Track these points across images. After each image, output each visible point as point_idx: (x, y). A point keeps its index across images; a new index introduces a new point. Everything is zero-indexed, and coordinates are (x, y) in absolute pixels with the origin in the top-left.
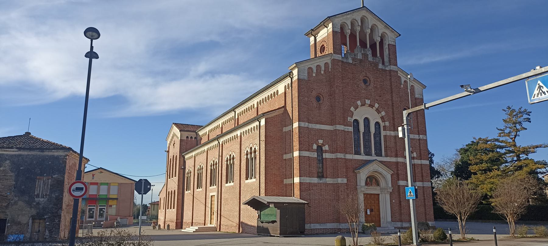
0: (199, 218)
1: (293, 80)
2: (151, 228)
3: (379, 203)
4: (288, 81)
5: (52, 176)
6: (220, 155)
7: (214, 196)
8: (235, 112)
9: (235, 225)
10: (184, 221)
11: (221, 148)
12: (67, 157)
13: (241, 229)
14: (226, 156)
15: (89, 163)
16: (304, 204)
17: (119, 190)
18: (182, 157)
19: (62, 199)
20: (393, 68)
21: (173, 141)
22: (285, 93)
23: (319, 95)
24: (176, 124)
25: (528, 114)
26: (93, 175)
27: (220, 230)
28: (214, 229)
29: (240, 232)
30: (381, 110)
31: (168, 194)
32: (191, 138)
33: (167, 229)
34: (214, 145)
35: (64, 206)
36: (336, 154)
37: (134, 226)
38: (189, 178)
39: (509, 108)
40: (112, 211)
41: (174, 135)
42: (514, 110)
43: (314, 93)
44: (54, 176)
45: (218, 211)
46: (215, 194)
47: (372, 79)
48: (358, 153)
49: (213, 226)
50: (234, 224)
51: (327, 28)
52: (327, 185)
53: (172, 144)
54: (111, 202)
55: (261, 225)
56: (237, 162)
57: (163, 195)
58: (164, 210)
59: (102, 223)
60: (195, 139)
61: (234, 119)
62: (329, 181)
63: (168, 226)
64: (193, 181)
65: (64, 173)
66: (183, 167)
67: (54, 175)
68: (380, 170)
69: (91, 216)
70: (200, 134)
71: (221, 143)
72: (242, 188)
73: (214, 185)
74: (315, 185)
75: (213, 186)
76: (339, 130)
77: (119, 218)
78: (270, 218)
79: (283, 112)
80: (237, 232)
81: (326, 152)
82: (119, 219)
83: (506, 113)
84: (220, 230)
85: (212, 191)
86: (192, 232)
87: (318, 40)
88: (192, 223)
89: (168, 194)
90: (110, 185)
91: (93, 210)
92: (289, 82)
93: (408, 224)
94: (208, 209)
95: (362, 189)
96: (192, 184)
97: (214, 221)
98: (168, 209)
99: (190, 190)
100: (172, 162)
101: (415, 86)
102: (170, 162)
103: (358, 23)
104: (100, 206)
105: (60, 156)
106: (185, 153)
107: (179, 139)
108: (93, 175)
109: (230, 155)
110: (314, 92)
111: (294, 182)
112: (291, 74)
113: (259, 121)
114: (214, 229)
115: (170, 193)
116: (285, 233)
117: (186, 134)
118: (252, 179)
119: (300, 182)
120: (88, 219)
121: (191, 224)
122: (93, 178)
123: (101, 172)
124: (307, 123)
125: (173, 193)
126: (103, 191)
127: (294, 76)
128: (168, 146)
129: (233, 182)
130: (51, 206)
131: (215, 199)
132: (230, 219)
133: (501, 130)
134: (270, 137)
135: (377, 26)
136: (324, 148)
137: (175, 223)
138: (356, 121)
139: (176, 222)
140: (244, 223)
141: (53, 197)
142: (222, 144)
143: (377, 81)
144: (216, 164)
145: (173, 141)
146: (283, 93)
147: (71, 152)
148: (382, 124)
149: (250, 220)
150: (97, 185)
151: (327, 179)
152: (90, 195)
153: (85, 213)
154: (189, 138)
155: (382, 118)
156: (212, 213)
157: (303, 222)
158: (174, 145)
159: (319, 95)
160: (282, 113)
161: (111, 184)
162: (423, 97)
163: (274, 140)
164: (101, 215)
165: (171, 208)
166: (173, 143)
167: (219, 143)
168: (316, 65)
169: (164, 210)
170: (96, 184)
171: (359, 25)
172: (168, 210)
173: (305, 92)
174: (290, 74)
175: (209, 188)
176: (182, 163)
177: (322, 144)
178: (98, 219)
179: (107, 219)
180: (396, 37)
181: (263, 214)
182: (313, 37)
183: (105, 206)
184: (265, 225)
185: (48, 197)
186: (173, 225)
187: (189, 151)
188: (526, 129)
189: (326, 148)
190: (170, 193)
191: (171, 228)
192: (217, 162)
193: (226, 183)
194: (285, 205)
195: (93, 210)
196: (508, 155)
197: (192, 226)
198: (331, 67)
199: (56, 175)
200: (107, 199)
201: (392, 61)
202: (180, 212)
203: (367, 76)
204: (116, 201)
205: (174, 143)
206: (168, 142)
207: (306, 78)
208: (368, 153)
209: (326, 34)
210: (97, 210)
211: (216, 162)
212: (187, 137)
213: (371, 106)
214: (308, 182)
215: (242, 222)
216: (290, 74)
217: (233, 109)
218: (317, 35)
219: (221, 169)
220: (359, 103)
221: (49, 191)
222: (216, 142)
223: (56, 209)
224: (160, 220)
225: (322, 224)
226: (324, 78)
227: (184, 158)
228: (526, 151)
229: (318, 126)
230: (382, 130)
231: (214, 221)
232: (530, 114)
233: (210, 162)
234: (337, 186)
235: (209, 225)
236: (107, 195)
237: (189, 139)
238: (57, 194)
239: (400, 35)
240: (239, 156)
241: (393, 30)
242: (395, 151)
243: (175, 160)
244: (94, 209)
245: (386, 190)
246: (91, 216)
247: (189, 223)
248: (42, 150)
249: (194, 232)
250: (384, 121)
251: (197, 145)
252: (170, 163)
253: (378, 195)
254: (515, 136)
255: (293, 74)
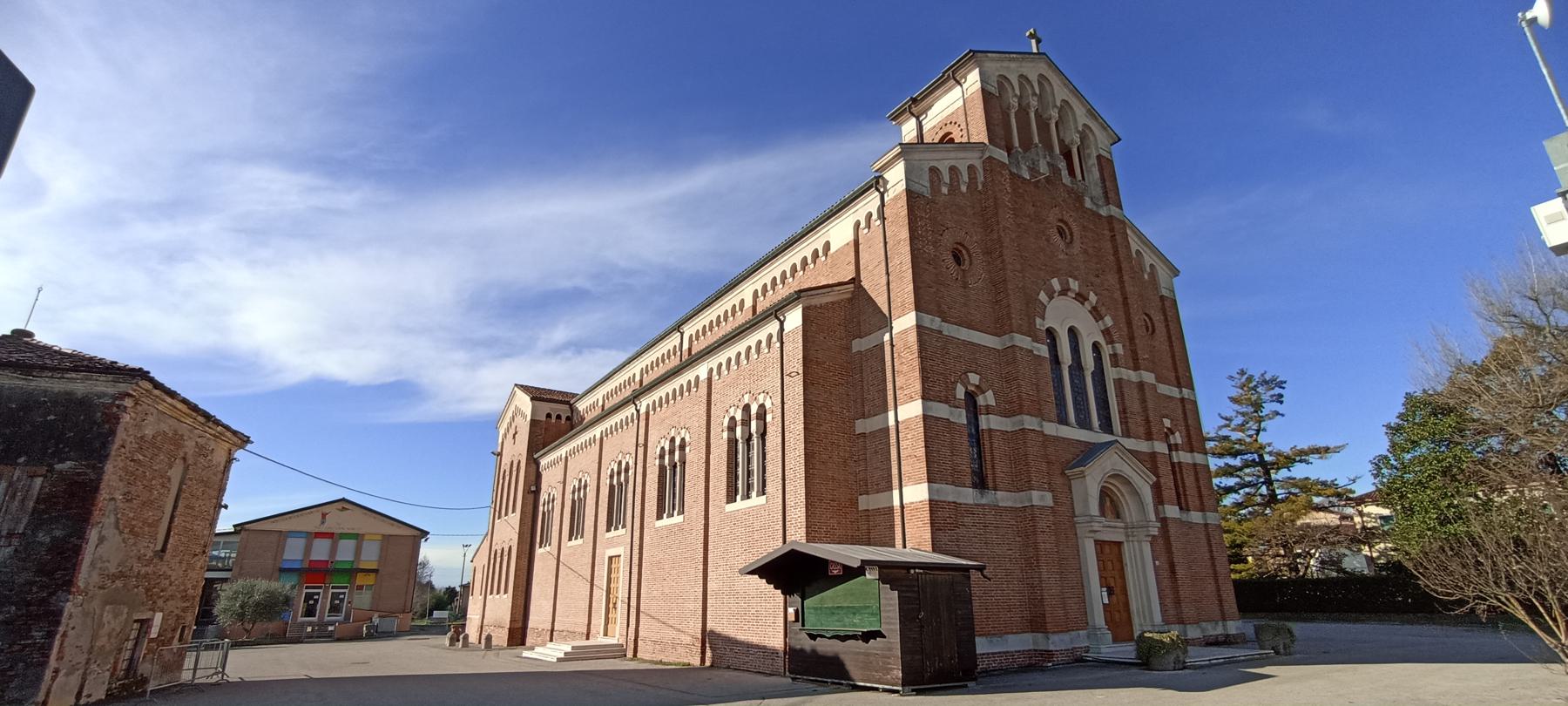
0: (572, 616)
1: (886, 199)
2: (446, 640)
3: (1122, 569)
4: (871, 202)
5: (51, 466)
6: (641, 440)
7: (619, 556)
8: (682, 334)
9: (687, 639)
10: (531, 624)
11: (642, 424)
12: (128, 402)
13: (709, 654)
14: (658, 442)
15: (249, 447)
16: (966, 569)
17: (383, 550)
18: (533, 462)
19: (77, 551)
20: (1114, 210)
21: (513, 427)
22: (856, 243)
23: (960, 248)
24: (522, 386)
25: (1281, 384)
26: (324, 516)
27: (635, 654)
28: (618, 651)
29: (708, 663)
30: (1103, 310)
31: (493, 556)
32: (559, 417)
33: (486, 647)
34: (622, 420)
35: (85, 575)
36: (1019, 417)
37: (412, 635)
38: (549, 514)
39: (1242, 373)
40: (363, 600)
41: (518, 412)
42: (1250, 379)
43: (948, 240)
44: (58, 467)
45: (629, 598)
46: (621, 550)
47: (1075, 229)
48: (1063, 420)
49: (614, 641)
50: (683, 637)
51: (961, 86)
52: (996, 508)
53: (510, 436)
54: (361, 579)
55: (807, 644)
56: (694, 456)
57: (483, 559)
58: (482, 598)
59: (331, 628)
60: (568, 422)
61: (679, 353)
62: (1004, 498)
63: (489, 638)
64: (559, 521)
65: (104, 458)
66: (533, 488)
67: (62, 461)
68: (1128, 471)
69: (310, 612)
70: (580, 409)
71: (643, 410)
72: (711, 530)
73: (620, 527)
74: (969, 510)
75: (616, 528)
76: (1021, 349)
77: (376, 615)
78: (846, 620)
79: (849, 296)
80: (696, 662)
81: (988, 410)
82: (376, 620)
83: (1233, 383)
84: (635, 654)
85: (612, 543)
86: (555, 660)
87: (925, 129)
88: (552, 631)
89: (492, 556)
90: (363, 540)
91: (316, 597)
92: (877, 202)
93: (1199, 631)
94: (600, 595)
95: (1093, 524)
96: (556, 528)
97: (618, 628)
98: (491, 593)
99: (549, 545)
100: (507, 478)
101: (1158, 268)
102: (504, 478)
103: (1032, 87)
104: (333, 588)
105: (96, 395)
106: (542, 452)
107: (529, 418)
108: (324, 516)
109: (673, 440)
110: (947, 235)
111: (904, 502)
112: (881, 181)
113: (779, 320)
114: (618, 652)
115: (499, 555)
116: (918, 679)
117: (547, 407)
118: (735, 501)
119: (930, 500)
120: (300, 619)
121: (549, 632)
122: (323, 523)
123: (344, 509)
124: (937, 318)
125: (506, 553)
126: (345, 552)
127: (888, 187)
128: (500, 441)
129: (681, 512)
130: (25, 576)
131: (622, 567)
132: (670, 623)
133: (1226, 419)
134: (818, 363)
135: (1071, 108)
136: (981, 400)
137: (507, 631)
138: (1051, 333)
139: (510, 629)
140: (719, 635)
141: (42, 544)
142: (647, 413)
143: (1086, 236)
144: (627, 470)
145: (513, 427)
146: (848, 244)
147: (147, 385)
148: (1106, 351)
149: (746, 628)
150: (332, 538)
151: (998, 492)
152: (311, 561)
153: (291, 603)
154: (554, 417)
155: (1106, 332)
156: (611, 605)
157: (966, 632)
158: (514, 437)
159: (960, 248)
160: (848, 299)
161: (366, 537)
162: (1174, 296)
163: (828, 373)
164: (335, 609)
165: (498, 593)
166: (512, 431)
167: (638, 411)
168: (948, 163)
169: (480, 597)
170: (330, 535)
171: (1034, 94)
172: (491, 596)
173: (927, 231)
174: (877, 183)
175: (603, 535)
176: (533, 478)
177: (977, 387)
178: (327, 619)
179: (347, 618)
180: (1111, 142)
181: (816, 609)
182: (913, 122)
183: (346, 587)
184: (825, 646)
185: (15, 542)
186: (501, 637)
187: (552, 445)
188: (1283, 415)
189: (987, 399)
190: (499, 555)
191: (494, 642)
192: (631, 464)
193: (658, 519)
194: (912, 571)
195: (342, 596)
196: (1247, 471)
197: (551, 640)
198: (982, 179)
199: (68, 462)
200: (352, 572)
201: (1112, 195)
202: (521, 602)
203: (1065, 219)
204: (373, 575)
205: (516, 433)
206: (502, 431)
207: (926, 192)
208: (1084, 423)
209: (961, 103)
210: (325, 597)
211: (627, 463)
212: (549, 416)
213: (1081, 298)
214: (951, 499)
215: (712, 632)
216: (878, 183)
217: (678, 327)
218: (924, 116)
219: (641, 481)
220: (1056, 284)
221: (25, 521)
222: (631, 410)
223: (42, 587)
224: (470, 622)
225: (995, 639)
226: (969, 204)
227: (538, 464)
228: (1288, 461)
229: (964, 334)
230: (1109, 365)
231: (618, 628)
232: (1284, 385)
233: (609, 466)
234: (1027, 514)
235: (599, 639)
236: (353, 562)
237: (553, 420)
238: (58, 533)
239: (1120, 140)
240: (705, 435)
241: (1105, 126)
242: (1143, 422)
243: (514, 473)
244: (318, 594)
245: (1145, 529)
246: (310, 612)
247: (543, 630)
248: (25, 369)
249: (559, 660)
250: (1111, 342)
251: (572, 429)
252: (501, 483)
253: (1119, 544)
254: (1258, 431)
255: (886, 182)
